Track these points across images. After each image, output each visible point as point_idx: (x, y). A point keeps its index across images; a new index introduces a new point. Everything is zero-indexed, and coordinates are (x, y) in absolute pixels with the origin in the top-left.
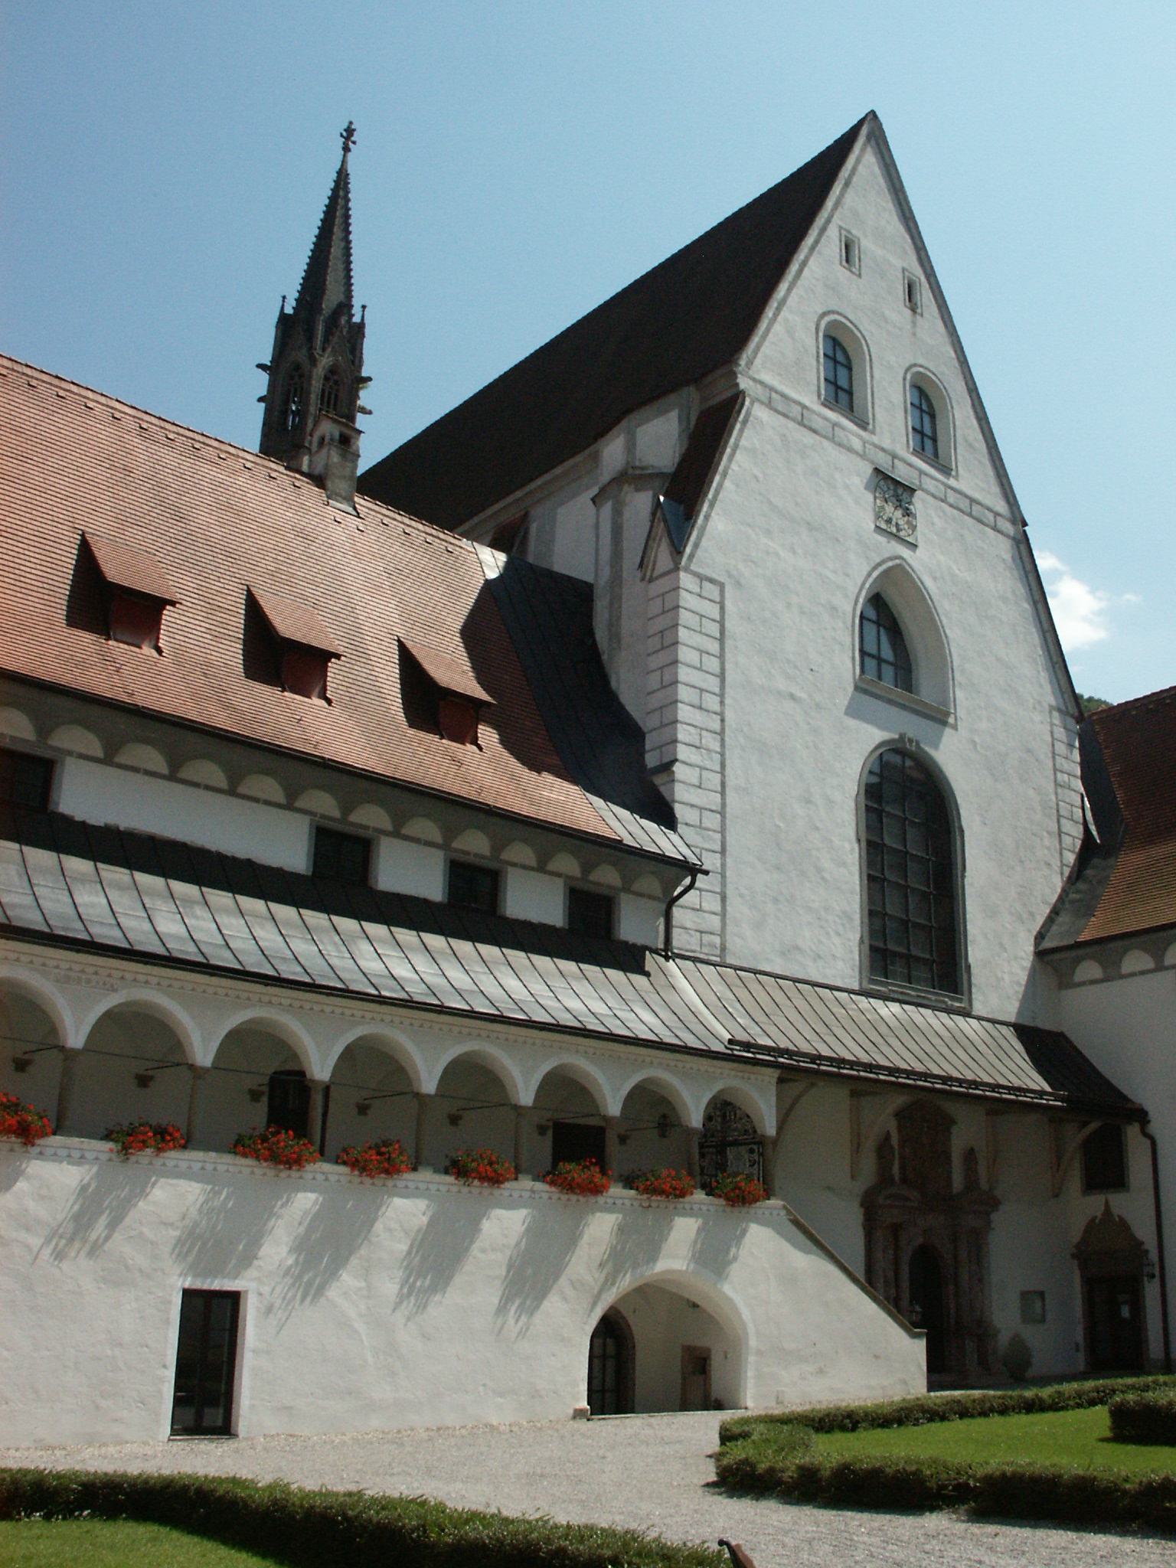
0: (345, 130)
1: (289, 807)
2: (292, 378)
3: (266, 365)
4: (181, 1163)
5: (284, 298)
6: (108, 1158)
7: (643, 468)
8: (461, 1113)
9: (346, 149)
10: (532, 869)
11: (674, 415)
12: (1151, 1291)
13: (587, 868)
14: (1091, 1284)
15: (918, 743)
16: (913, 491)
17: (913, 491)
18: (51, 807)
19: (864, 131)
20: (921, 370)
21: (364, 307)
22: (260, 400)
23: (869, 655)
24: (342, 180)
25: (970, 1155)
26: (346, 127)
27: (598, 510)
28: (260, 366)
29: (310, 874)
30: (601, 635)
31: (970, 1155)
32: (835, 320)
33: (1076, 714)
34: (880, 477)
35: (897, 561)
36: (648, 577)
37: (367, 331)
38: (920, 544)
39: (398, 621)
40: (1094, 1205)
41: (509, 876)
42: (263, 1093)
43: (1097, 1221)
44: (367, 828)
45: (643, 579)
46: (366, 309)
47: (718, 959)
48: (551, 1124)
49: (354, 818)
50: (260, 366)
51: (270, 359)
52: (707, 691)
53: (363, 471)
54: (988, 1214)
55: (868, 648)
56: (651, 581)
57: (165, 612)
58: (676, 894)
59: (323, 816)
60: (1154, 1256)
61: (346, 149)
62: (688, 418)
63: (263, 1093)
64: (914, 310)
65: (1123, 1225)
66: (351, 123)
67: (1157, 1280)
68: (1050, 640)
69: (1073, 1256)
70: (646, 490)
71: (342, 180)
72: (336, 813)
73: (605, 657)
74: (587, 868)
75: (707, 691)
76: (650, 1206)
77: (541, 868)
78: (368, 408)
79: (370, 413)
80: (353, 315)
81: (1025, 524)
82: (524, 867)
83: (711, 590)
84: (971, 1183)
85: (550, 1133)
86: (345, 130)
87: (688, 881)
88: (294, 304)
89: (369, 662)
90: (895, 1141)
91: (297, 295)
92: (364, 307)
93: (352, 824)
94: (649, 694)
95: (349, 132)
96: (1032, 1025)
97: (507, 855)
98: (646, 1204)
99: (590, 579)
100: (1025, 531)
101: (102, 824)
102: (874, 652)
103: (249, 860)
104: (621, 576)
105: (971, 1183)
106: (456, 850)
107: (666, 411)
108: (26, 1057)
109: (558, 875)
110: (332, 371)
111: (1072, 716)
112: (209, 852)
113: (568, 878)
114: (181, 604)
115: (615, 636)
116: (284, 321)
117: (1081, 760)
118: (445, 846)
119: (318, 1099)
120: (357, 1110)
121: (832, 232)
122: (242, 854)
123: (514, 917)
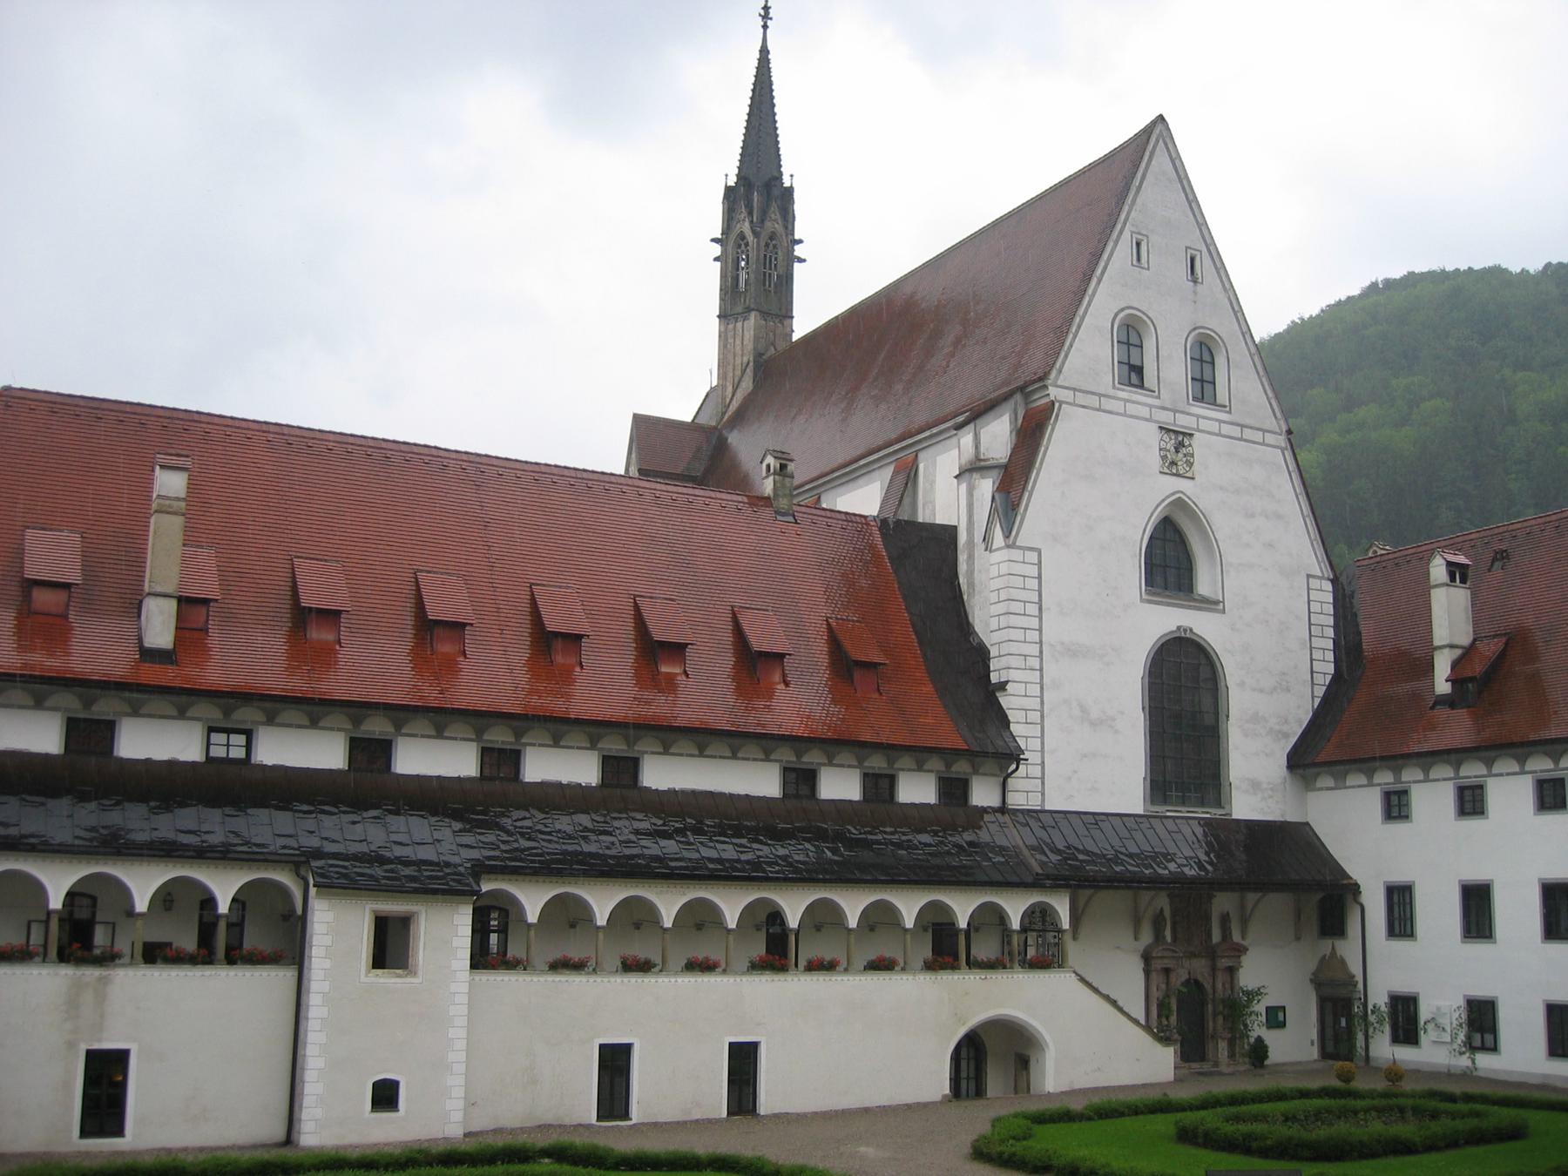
0: (763, 8)
2: (740, 246)
3: (719, 239)
5: (727, 175)
7: (984, 460)
10: (914, 770)
13: (948, 766)
14: (1323, 1002)
15: (1191, 630)
16: (1191, 435)
17: (1191, 435)
18: (640, 784)
19: (1157, 132)
20: (1202, 331)
21: (792, 176)
22: (716, 259)
24: (764, 52)
26: (763, 5)
27: (958, 485)
28: (713, 240)
29: (781, 796)
30: (962, 580)
32: (1132, 314)
34: (1163, 432)
35: (1178, 495)
37: (795, 190)
38: (1196, 477)
41: (900, 779)
45: (986, 550)
46: (794, 178)
47: (1039, 808)
48: (930, 925)
50: (713, 240)
51: (720, 232)
52: (1029, 629)
53: (800, 337)
54: (1239, 957)
56: (991, 551)
57: (687, 650)
58: (1009, 771)
60: (1360, 986)
62: (1016, 419)
64: (1195, 281)
65: (1343, 962)
71: (764, 52)
73: (965, 597)
74: (948, 766)
75: (1029, 629)
76: (986, 978)
78: (803, 257)
79: (804, 261)
82: (909, 770)
86: (763, 8)
87: (1014, 766)
88: (735, 179)
90: (1167, 913)
91: (736, 171)
92: (792, 176)
94: (992, 632)
95: (766, 8)
96: (1283, 820)
98: (983, 977)
99: (954, 523)
101: (666, 789)
103: (747, 795)
104: (973, 541)
109: (932, 771)
112: (725, 794)
113: (938, 772)
114: (691, 644)
115: (971, 585)
116: (729, 191)
117: (1334, 624)
119: (792, 938)
121: (1126, 234)
122: (743, 792)
123: (904, 802)
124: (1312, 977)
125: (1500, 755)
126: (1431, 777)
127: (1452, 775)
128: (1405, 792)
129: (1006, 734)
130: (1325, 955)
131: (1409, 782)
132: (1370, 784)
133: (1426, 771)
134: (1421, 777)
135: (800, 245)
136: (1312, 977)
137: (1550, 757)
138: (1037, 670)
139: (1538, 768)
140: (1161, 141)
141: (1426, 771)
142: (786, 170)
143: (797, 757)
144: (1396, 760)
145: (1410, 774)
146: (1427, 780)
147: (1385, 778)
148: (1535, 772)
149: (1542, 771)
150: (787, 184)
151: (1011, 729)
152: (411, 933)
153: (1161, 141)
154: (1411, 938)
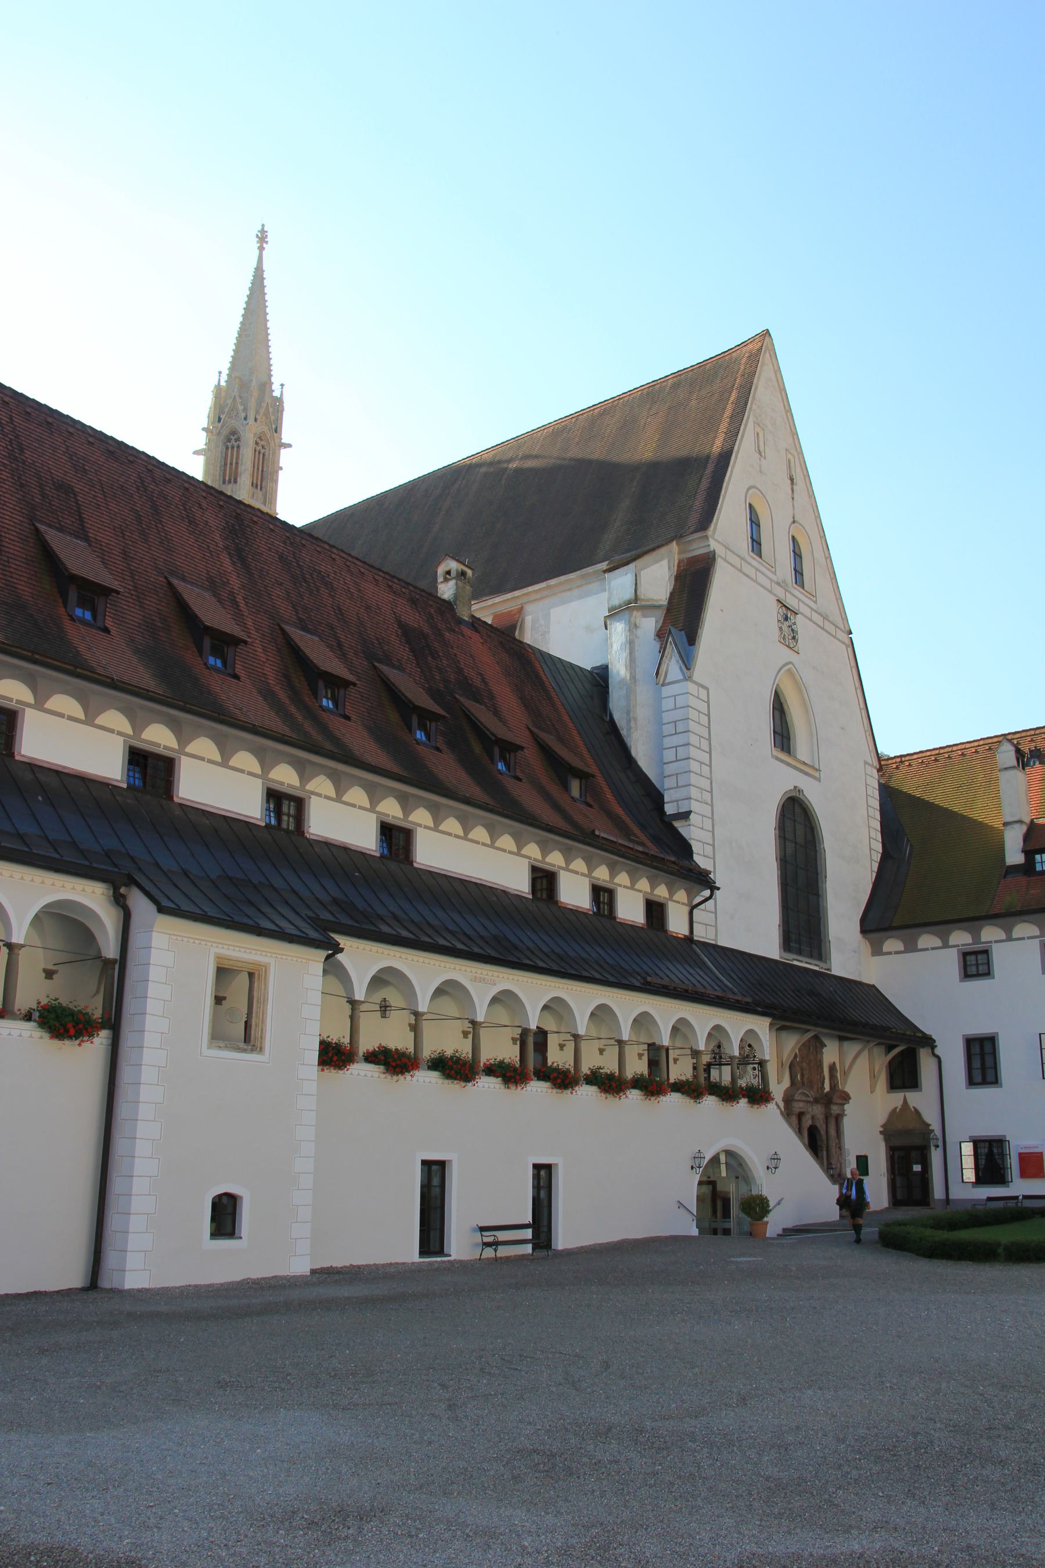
1: (518, 854)
4: (13, 1032)
6: (39, 1036)
7: (648, 600)
8: (605, 1047)
9: (261, 249)
11: (665, 563)
12: (936, 1157)
21: (282, 385)
23: (778, 734)
25: (832, 1068)
31: (832, 1068)
33: (878, 767)
36: (661, 683)
39: (16, 539)
40: (896, 1099)
42: (470, 1033)
43: (898, 1110)
44: (554, 866)
49: (549, 859)
55: (777, 730)
59: (535, 860)
60: (938, 1132)
61: (261, 249)
63: (470, 1033)
66: (263, 226)
67: (940, 1150)
68: (864, 715)
69: (881, 1132)
70: (652, 617)
72: (607, 878)
77: (632, 887)
80: (273, 391)
81: (851, 633)
83: (703, 694)
84: (834, 1086)
85: (518, 1042)
89: (255, 657)
92: (282, 385)
93: (656, 895)
97: (617, 880)
100: (851, 638)
102: (780, 732)
105: (834, 1086)
106: (594, 878)
107: (661, 560)
108: (564, 1042)
109: (641, 891)
110: (260, 437)
111: (875, 767)
118: (589, 875)
120: (44, 975)
124: (881, 1129)
125: (888, 938)
126: (1014, 936)
127: (941, 945)
128: (986, 952)
129: (693, 863)
130: (896, 1108)
131: (991, 942)
132: (946, 945)
133: (1008, 931)
134: (1003, 936)
135: (288, 449)
136: (881, 1129)
137: (871, 944)
138: (678, 805)
139: (960, 942)
140: (767, 352)
141: (1008, 931)
142: (276, 381)
143: (518, 848)
144: (973, 920)
145: (990, 933)
146: (1009, 939)
147: (961, 938)
148: (958, 946)
149: (962, 945)
150: (277, 394)
151: (694, 858)
152: (553, 582)
153: (767, 352)
154: (996, 1085)
